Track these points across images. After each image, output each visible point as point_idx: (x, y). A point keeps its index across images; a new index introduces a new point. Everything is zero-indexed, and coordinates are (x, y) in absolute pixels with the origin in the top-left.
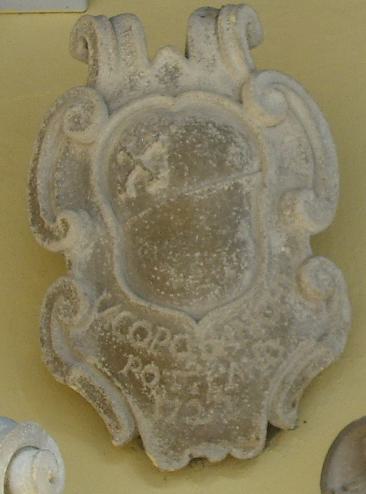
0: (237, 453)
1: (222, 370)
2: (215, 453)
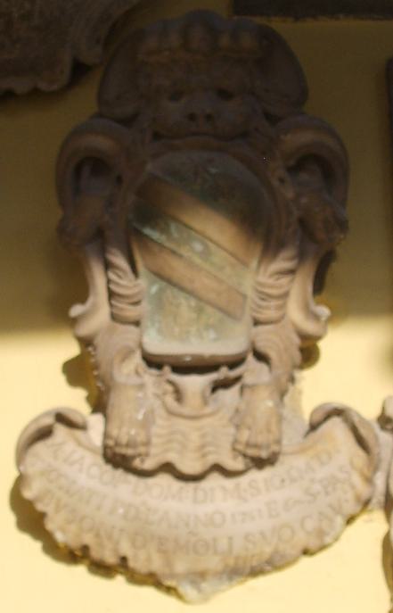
0: (43, 86)
1: (27, 6)
2: (21, 85)
